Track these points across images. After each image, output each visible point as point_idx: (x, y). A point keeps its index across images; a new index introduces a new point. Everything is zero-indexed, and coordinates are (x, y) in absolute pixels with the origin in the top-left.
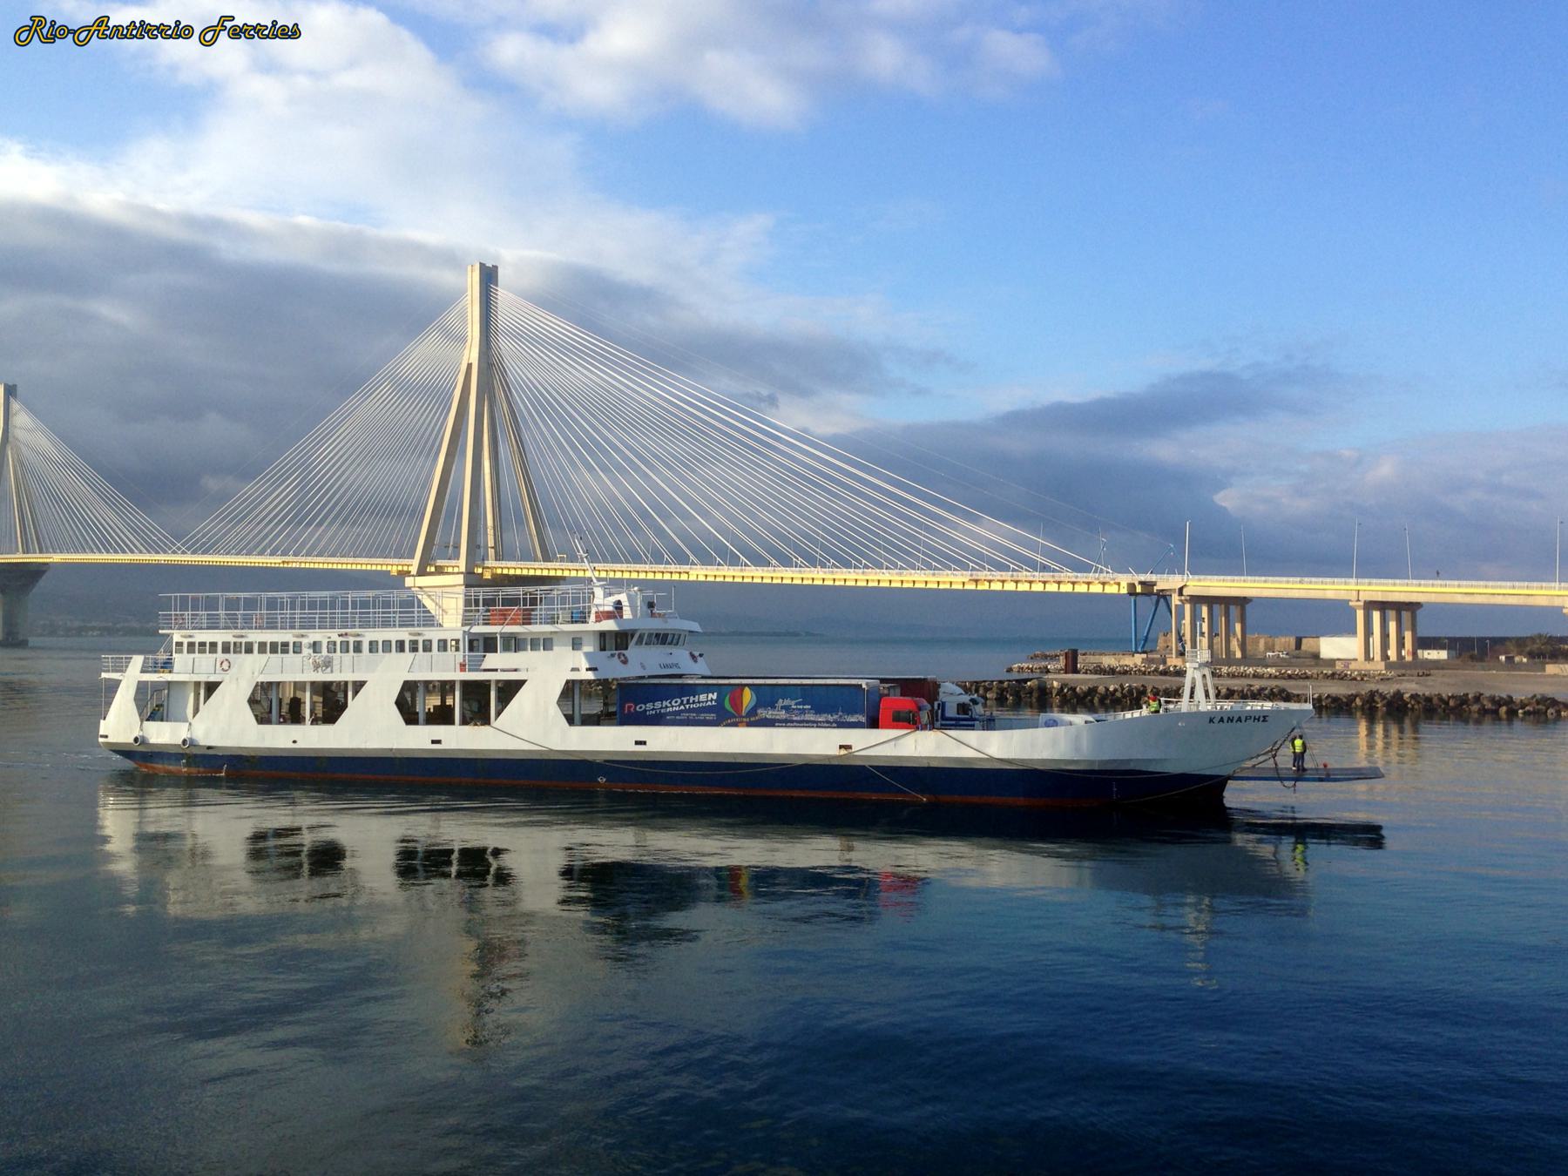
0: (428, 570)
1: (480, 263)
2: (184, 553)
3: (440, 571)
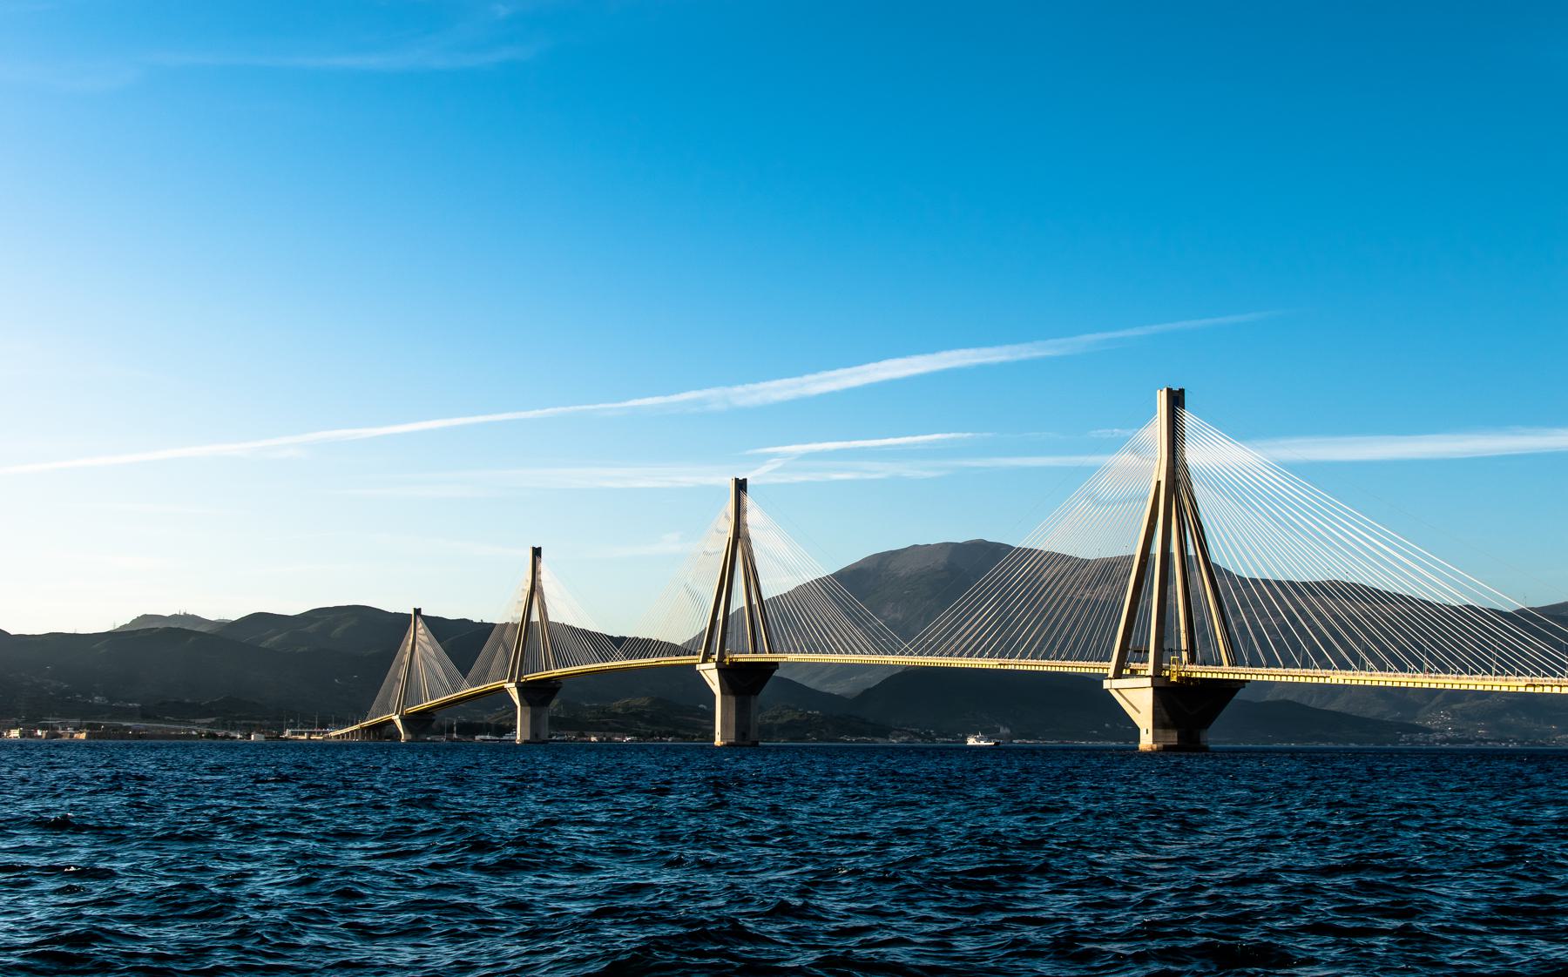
0: (1124, 672)
1: (1168, 389)
2: (911, 654)
3: (1134, 673)
